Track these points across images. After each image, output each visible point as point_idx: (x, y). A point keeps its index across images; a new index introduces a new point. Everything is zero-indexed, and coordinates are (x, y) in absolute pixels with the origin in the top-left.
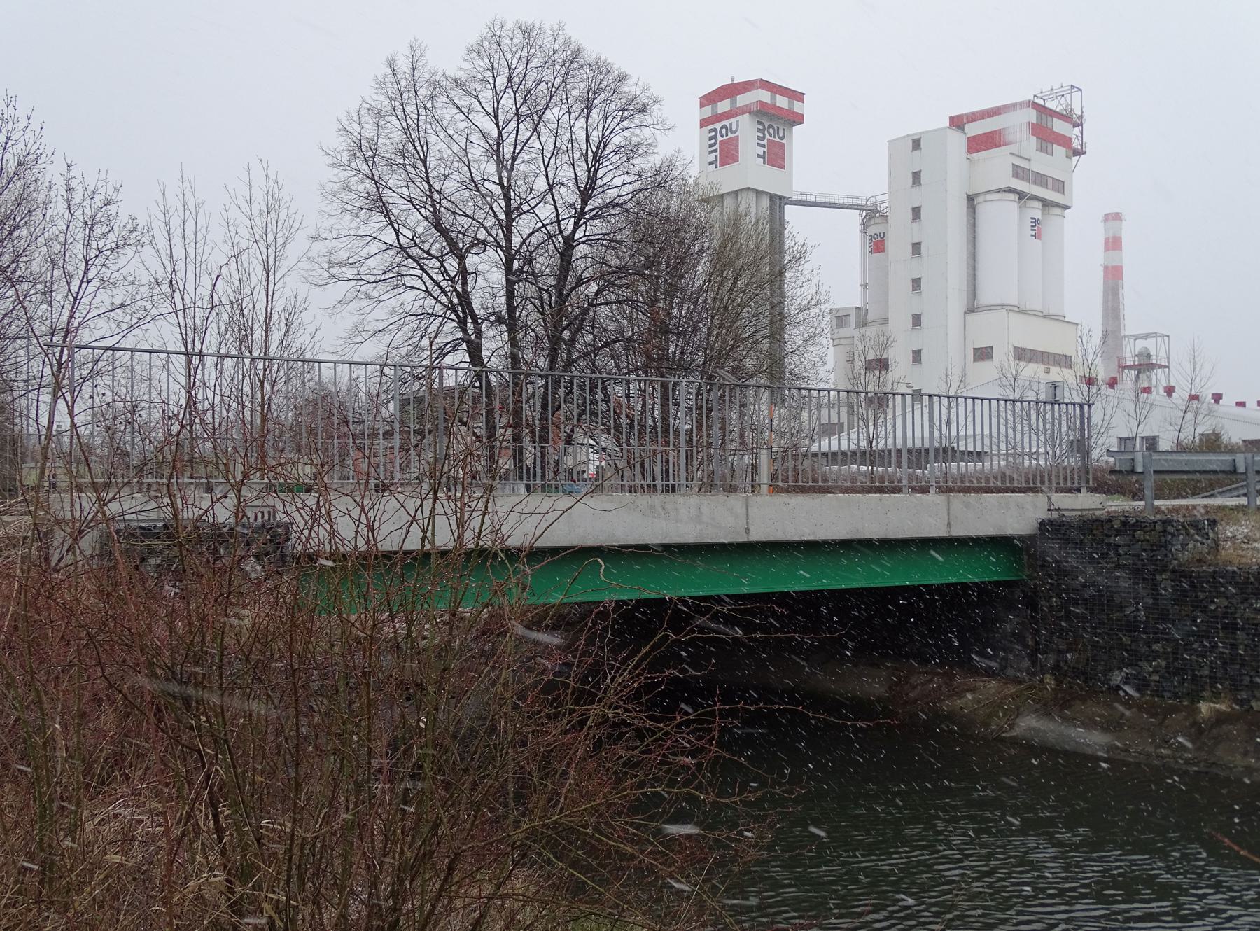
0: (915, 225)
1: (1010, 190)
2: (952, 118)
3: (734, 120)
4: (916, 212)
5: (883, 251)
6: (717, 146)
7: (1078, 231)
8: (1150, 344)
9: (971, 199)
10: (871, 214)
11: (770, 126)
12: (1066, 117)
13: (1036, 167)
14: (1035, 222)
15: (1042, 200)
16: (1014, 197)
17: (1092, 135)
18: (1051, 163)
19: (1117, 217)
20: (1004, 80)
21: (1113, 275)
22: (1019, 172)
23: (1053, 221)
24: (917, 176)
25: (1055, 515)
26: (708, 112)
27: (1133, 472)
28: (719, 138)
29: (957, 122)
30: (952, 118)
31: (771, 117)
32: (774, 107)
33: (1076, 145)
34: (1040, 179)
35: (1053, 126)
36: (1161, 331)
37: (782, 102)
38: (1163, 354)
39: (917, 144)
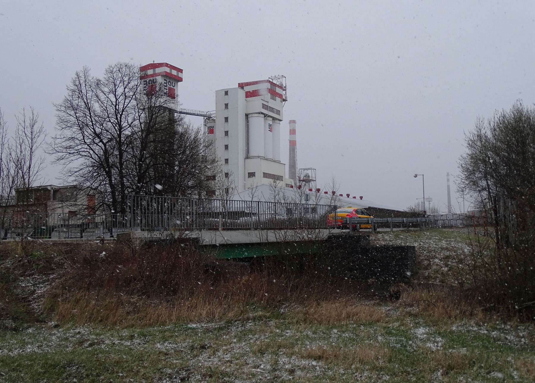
1: (262, 113)
2: (239, 84)
4: (226, 119)
5: (213, 133)
7: (283, 128)
8: (309, 172)
9: (247, 115)
10: (208, 118)
11: (169, 82)
12: (281, 87)
13: (270, 105)
14: (270, 125)
15: (272, 117)
16: (263, 116)
17: (289, 94)
18: (275, 104)
19: (294, 122)
20: (258, 73)
21: (293, 144)
22: (265, 107)
23: (276, 125)
24: (226, 105)
25: (331, 235)
27: (346, 223)
29: (241, 86)
30: (239, 84)
31: (170, 78)
33: (284, 98)
34: (272, 109)
35: (276, 90)
36: (313, 167)
37: (174, 72)
38: (314, 176)
39: (226, 93)
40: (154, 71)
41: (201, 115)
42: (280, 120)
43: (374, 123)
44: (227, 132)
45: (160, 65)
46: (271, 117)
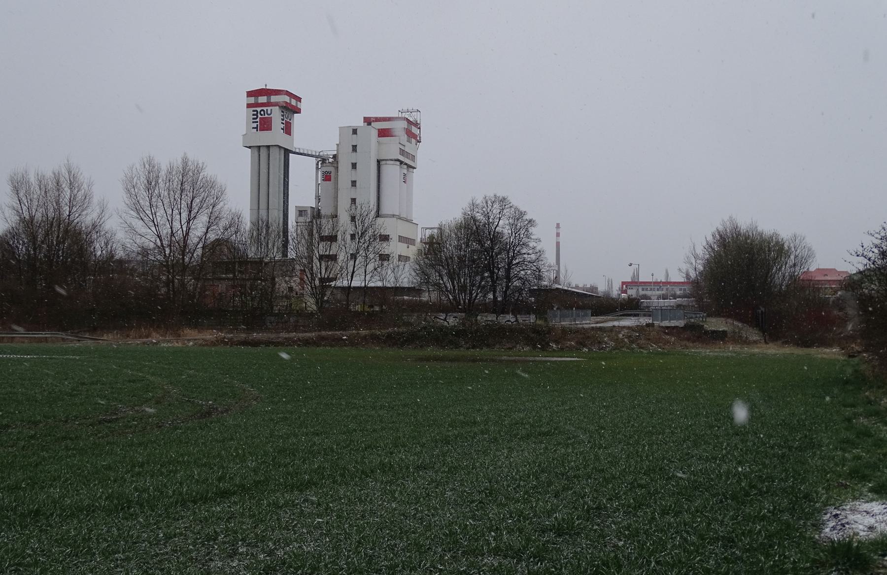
0: (353, 171)
1: (398, 160)
3: (269, 109)
6: (258, 120)
9: (379, 162)
16: (398, 163)
20: (385, 107)
26: (252, 100)
28: (259, 116)
32: (290, 104)
35: (412, 130)
37: (294, 102)
39: (355, 132)
40: (269, 99)
41: (312, 156)
42: (414, 168)
43: (833, 251)
44: (355, 182)
45: (277, 92)
46: (406, 164)
